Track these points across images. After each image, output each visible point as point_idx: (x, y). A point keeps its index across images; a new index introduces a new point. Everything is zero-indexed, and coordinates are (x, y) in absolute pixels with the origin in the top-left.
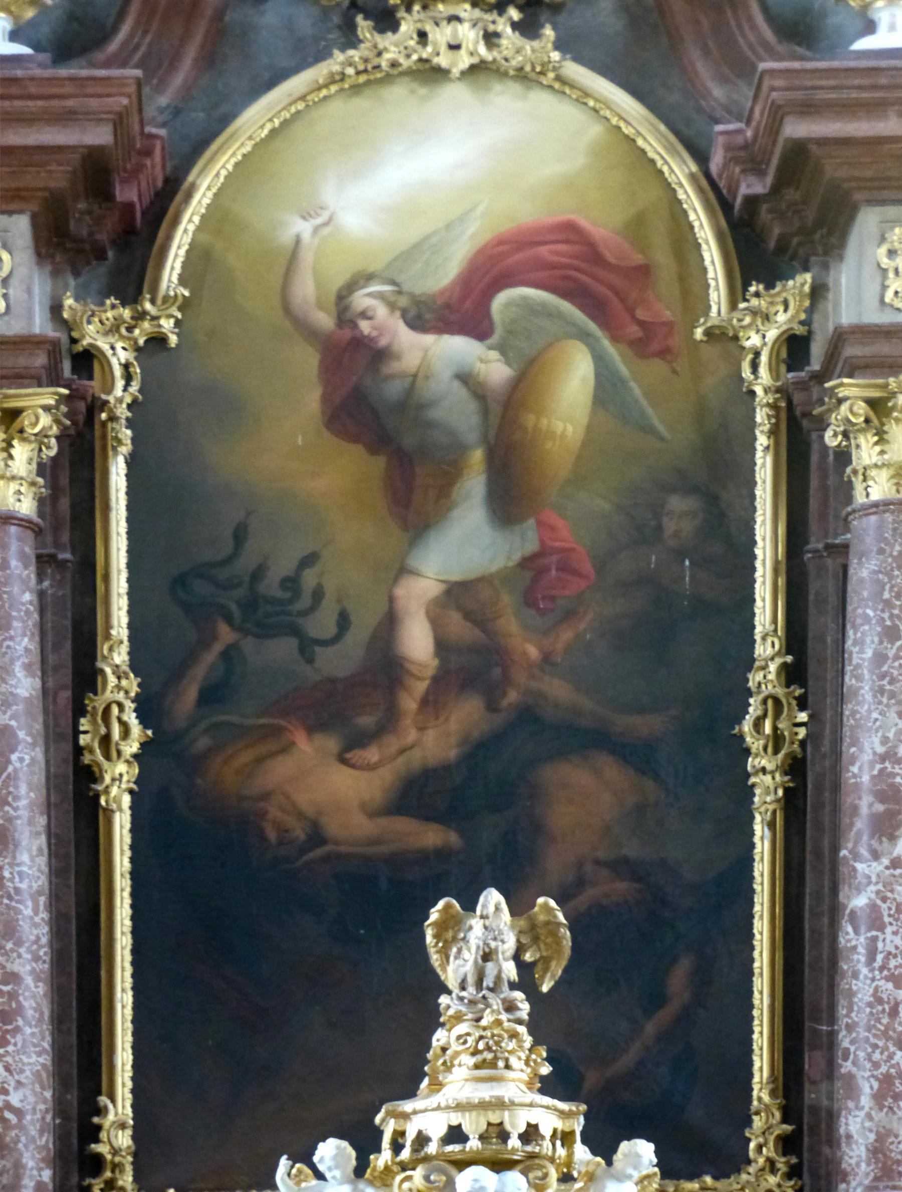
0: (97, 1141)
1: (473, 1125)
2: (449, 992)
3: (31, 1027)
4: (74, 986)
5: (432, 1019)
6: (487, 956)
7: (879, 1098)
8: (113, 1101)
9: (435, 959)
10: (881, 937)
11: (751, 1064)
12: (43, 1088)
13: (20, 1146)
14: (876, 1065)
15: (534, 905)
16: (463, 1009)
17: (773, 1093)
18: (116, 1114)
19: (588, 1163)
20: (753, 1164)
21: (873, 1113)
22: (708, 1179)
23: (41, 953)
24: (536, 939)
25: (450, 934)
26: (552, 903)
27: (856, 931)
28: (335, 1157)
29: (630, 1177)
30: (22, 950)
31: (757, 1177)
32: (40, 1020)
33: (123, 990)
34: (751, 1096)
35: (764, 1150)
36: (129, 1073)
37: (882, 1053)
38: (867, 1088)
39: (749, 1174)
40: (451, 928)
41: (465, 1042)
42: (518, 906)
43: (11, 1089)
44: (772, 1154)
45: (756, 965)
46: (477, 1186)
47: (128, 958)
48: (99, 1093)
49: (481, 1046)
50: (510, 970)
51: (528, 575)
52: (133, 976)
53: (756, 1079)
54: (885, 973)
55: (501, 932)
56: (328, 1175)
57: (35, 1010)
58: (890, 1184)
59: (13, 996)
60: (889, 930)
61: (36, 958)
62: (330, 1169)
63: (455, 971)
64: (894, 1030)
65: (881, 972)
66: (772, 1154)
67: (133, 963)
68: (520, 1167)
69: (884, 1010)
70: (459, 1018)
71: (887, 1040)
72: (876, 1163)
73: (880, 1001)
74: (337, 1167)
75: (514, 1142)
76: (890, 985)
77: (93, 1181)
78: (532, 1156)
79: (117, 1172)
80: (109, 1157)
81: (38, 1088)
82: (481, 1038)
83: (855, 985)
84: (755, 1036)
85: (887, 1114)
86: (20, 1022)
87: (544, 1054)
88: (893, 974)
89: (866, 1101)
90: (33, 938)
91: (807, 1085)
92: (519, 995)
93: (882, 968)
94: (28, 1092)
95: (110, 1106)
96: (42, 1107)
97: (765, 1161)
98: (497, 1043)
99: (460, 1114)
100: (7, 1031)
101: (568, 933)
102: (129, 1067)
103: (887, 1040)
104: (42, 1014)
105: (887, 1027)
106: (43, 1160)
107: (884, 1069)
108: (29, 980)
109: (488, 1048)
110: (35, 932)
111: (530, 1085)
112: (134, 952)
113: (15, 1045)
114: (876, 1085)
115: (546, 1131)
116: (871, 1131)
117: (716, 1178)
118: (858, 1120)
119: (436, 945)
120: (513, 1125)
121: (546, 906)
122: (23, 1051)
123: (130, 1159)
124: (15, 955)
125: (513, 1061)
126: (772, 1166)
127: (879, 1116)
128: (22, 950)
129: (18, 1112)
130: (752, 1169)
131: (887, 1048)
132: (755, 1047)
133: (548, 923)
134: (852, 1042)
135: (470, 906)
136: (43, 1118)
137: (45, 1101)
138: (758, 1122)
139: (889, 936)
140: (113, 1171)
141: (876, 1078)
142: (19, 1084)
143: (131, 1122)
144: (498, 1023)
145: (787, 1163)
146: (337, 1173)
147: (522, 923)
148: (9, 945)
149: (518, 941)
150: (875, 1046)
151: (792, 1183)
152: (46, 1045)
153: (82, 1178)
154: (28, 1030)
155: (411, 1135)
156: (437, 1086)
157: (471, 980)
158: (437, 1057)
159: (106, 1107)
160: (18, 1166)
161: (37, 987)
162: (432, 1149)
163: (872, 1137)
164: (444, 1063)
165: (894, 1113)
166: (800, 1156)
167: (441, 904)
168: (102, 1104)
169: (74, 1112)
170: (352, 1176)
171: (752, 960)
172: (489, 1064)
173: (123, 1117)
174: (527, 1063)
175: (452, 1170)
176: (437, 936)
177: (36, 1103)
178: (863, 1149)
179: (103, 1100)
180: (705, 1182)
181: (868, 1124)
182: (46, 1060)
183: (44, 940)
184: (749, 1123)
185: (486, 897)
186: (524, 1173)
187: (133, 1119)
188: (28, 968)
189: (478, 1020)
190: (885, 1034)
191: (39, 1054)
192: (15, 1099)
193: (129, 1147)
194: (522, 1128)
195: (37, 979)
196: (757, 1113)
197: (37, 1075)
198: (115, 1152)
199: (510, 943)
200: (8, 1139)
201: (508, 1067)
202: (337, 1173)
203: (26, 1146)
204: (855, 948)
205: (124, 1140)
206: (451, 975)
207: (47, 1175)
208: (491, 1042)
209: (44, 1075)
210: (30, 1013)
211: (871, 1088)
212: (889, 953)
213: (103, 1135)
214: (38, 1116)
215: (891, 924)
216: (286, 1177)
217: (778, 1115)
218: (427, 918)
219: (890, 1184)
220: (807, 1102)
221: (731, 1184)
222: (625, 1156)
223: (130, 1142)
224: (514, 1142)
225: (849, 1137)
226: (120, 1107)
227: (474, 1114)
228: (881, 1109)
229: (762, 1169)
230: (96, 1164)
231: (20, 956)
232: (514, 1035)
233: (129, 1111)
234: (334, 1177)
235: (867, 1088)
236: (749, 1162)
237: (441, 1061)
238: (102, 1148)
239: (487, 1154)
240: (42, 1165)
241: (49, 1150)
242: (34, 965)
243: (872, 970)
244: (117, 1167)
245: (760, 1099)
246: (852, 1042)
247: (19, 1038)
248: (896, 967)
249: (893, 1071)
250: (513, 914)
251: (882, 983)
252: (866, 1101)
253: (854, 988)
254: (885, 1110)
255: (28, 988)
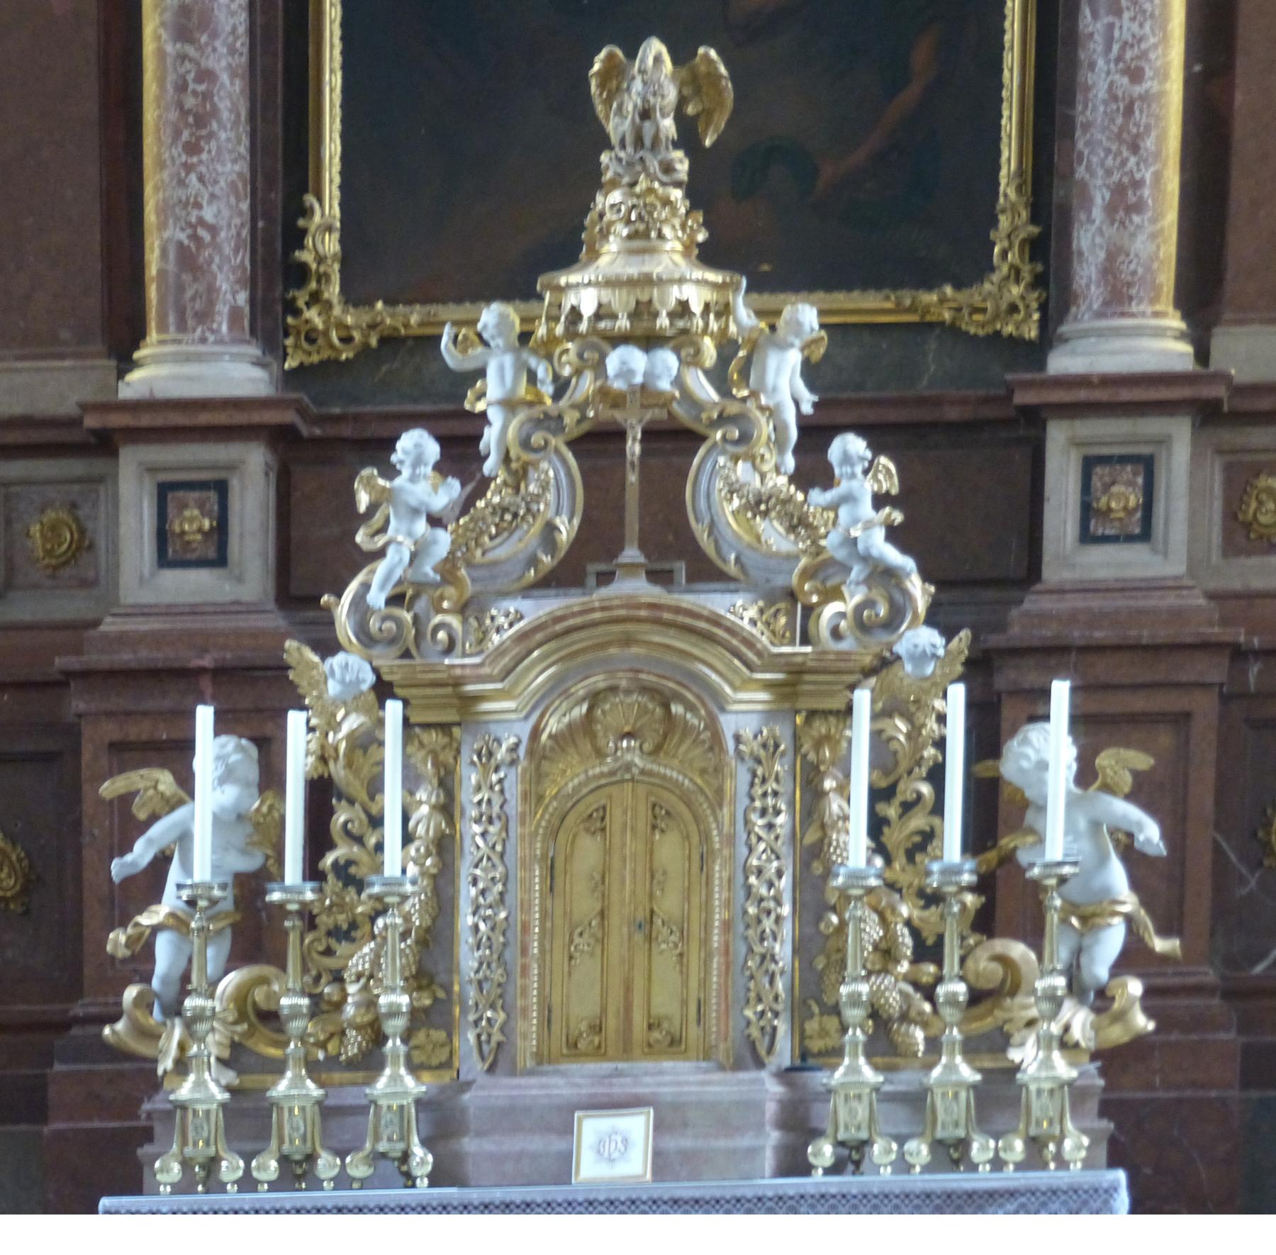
0: (302, 247)
1: (621, 302)
2: (611, 148)
3: (226, 130)
4: (280, 66)
5: (594, 182)
6: (646, 114)
7: (1111, 209)
8: (320, 200)
9: (599, 108)
10: (1118, 25)
11: (998, 153)
12: (238, 200)
13: (214, 267)
14: (1109, 173)
15: (696, 54)
16: (620, 170)
17: (1019, 189)
18: (323, 214)
19: (752, 329)
20: (997, 273)
21: (1104, 228)
22: (949, 290)
23: (238, 44)
24: (698, 91)
25: (614, 83)
26: (713, 53)
27: (1095, 15)
28: (498, 325)
29: (792, 345)
30: (218, 44)
31: (1000, 288)
32: (236, 123)
33: (332, 71)
34: (998, 193)
35: (1010, 256)
36: (337, 167)
37: (1114, 159)
38: (1100, 197)
39: (992, 283)
40: (615, 76)
41: (619, 210)
42: (681, 55)
43: (205, 204)
44: (1017, 261)
45: (1007, 37)
46: (625, 368)
47: (338, 32)
48: (306, 191)
49: (633, 217)
50: (668, 125)
51: (61, 678)
52: (343, 53)
53: (1003, 172)
54: (1121, 65)
55: (661, 86)
56: (492, 344)
57: (231, 111)
58: (1119, 310)
59: (207, 96)
60: (1126, 15)
61: (232, 51)
62: (493, 338)
63: (616, 128)
64: (1129, 132)
65: (1116, 65)
66: (1017, 261)
67: (343, 38)
68: (672, 344)
69: (1118, 109)
70: (614, 184)
71: (1120, 144)
72: (1106, 286)
73: (1115, 98)
74: (500, 334)
75: (663, 321)
76: (1125, 80)
77: (297, 293)
78: (685, 332)
79: (323, 281)
80: (314, 266)
81: (233, 200)
82: (634, 206)
83: (1091, 78)
84: (1004, 122)
85: (1118, 229)
86: (215, 125)
87: (701, 220)
88: (1129, 67)
89: (1098, 213)
90: (228, 29)
91: (1056, 181)
92: (678, 154)
93: (1119, 59)
94: (222, 206)
95: (317, 206)
96: (237, 221)
97: (1010, 270)
98: (651, 214)
99: (610, 291)
100: (200, 137)
101: (730, 85)
102: (337, 160)
103: (1120, 144)
104: (238, 115)
105: (1122, 129)
106: (238, 281)
107: (1116, 177)
108: (225, 78)
109: (640, 217)
110: (231, 21)
111: (686, 253)
112: (344, 25)
113: (209, 151)
114: (1108, 196)
115: (697, 308)
116: (1101, 247)
117: (958, 286)
118: (1090, 235)
119: (601, 94)
120: (663, 304)
121: (706, 56)
122: (219, 157)
123: (337, 266)
124: (210, 49)
125: (667, 231)
126: (1016, 274)
127: (1111, 231)
128: (218, 44)
129: (213, 230)
130: (996, 277)
131: (1120, 153)
132: (1003, 134)
133: (709, 74)
134: (1087, 144)
135: (631, 54)
136: (239, 234)
137: (241, 213)
138: (1004, 222)
139: (1126, 23)
140: (319, 282)
141: (1108, 187)
142: (213, 197)
143: (338, 224)
144: (651, 190)
145: (1032, 271)
146: (500, 342)
147: (684, 73)
148: (204, 39)
149: (680, 92)
150: (1108, 151)
151: (1036, 295)
152: (243, 149)
153: (286, 290)
154: (223, 136)
155: (566, 308)
156: (595, 255)
157: (629, 140)
158: (594, 224)
159: (312, 210)
160: (212, 290)
161: (232, 84)
162: (583, 327)
163: (1102, 255)
164: (601, 230)
165: (1125, 228)
166: (1047, 264)
167: (602, 54)
168: (308, 204)
169: (279, 215)
170: (517, 343)
171: (1003, 32)
172: (643, 237)
173: (330, 220)
174: (683, 226)
175: (605, 346)
176: (602, 86)
177: (231, 217)
178: (1093, 268)
179: (310, 199)
180: (945, 294)
181: (1098, 240)
182: (243, 167)
183: (242, 30)
184: (994, 222)
185: (645, 51)
186: (677, 350)
187: (341, 222)
188: (224, 63)
189: (633, 184)
190: (1119, 137)
191: (234, 161)
192: (208, 214)
193: (335, 255)
194: (672, 303)
195: (233, 75)
196: (1003, 211)
197: (233, 185)
198: (320, 260)
199: (671, 94)
200: (201, 260)
201: (661, 236)
202: (500, 342)
203: (220, 268)
204: (1092, 35)
205: (331, 245)
206: (616, 127)
207: (242, 298)
208: (643, 213)
209: (240, 185)
210: (225, 115)
211: (1103, 199)
212: (1126, 43)
213: (309, 241)
214: (233, 231)
215: (1128, 9)
216: (451, 346)
217: (1024, 214)
218: (592, 66)
219: (1119, 310)
220: (1055, 200)
221: (972, 295)
222: (787, 323)
223: (338, 248)
224: (663, 321)
225: (1080, 254)
226: (328, 206)
227: (624, 291)
228: (1112, 223)
229: (1007, 278)
230: (300, 274)
231: (214, 50)
232: (667, 202)
233: (337, 211)
234: (498, 346)
235: (1100, 197)
236: (992, 269)
237: (597, 229)
238: (306, 256)
239: (639, 332)
240: (237, 287)
241: (245, 269)
242: (230, 59)
243: (1108, 62)
244: (323, 278)
245: (1006, 195)
246: (1087, 144)
247: (213, 144)
248: (1132, 59)
249: (1126, 180)
250: (675, 61)
251: (1117, 77)
252: (1098, 213)
253: (1090, 82)
254: (1116, 225)
255: (222, 85)
